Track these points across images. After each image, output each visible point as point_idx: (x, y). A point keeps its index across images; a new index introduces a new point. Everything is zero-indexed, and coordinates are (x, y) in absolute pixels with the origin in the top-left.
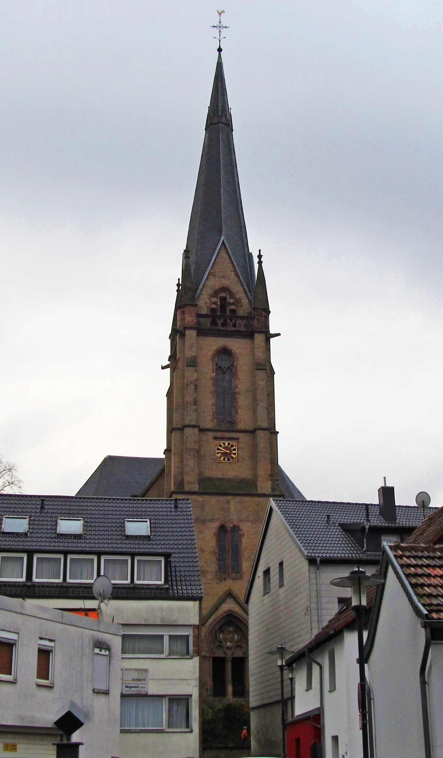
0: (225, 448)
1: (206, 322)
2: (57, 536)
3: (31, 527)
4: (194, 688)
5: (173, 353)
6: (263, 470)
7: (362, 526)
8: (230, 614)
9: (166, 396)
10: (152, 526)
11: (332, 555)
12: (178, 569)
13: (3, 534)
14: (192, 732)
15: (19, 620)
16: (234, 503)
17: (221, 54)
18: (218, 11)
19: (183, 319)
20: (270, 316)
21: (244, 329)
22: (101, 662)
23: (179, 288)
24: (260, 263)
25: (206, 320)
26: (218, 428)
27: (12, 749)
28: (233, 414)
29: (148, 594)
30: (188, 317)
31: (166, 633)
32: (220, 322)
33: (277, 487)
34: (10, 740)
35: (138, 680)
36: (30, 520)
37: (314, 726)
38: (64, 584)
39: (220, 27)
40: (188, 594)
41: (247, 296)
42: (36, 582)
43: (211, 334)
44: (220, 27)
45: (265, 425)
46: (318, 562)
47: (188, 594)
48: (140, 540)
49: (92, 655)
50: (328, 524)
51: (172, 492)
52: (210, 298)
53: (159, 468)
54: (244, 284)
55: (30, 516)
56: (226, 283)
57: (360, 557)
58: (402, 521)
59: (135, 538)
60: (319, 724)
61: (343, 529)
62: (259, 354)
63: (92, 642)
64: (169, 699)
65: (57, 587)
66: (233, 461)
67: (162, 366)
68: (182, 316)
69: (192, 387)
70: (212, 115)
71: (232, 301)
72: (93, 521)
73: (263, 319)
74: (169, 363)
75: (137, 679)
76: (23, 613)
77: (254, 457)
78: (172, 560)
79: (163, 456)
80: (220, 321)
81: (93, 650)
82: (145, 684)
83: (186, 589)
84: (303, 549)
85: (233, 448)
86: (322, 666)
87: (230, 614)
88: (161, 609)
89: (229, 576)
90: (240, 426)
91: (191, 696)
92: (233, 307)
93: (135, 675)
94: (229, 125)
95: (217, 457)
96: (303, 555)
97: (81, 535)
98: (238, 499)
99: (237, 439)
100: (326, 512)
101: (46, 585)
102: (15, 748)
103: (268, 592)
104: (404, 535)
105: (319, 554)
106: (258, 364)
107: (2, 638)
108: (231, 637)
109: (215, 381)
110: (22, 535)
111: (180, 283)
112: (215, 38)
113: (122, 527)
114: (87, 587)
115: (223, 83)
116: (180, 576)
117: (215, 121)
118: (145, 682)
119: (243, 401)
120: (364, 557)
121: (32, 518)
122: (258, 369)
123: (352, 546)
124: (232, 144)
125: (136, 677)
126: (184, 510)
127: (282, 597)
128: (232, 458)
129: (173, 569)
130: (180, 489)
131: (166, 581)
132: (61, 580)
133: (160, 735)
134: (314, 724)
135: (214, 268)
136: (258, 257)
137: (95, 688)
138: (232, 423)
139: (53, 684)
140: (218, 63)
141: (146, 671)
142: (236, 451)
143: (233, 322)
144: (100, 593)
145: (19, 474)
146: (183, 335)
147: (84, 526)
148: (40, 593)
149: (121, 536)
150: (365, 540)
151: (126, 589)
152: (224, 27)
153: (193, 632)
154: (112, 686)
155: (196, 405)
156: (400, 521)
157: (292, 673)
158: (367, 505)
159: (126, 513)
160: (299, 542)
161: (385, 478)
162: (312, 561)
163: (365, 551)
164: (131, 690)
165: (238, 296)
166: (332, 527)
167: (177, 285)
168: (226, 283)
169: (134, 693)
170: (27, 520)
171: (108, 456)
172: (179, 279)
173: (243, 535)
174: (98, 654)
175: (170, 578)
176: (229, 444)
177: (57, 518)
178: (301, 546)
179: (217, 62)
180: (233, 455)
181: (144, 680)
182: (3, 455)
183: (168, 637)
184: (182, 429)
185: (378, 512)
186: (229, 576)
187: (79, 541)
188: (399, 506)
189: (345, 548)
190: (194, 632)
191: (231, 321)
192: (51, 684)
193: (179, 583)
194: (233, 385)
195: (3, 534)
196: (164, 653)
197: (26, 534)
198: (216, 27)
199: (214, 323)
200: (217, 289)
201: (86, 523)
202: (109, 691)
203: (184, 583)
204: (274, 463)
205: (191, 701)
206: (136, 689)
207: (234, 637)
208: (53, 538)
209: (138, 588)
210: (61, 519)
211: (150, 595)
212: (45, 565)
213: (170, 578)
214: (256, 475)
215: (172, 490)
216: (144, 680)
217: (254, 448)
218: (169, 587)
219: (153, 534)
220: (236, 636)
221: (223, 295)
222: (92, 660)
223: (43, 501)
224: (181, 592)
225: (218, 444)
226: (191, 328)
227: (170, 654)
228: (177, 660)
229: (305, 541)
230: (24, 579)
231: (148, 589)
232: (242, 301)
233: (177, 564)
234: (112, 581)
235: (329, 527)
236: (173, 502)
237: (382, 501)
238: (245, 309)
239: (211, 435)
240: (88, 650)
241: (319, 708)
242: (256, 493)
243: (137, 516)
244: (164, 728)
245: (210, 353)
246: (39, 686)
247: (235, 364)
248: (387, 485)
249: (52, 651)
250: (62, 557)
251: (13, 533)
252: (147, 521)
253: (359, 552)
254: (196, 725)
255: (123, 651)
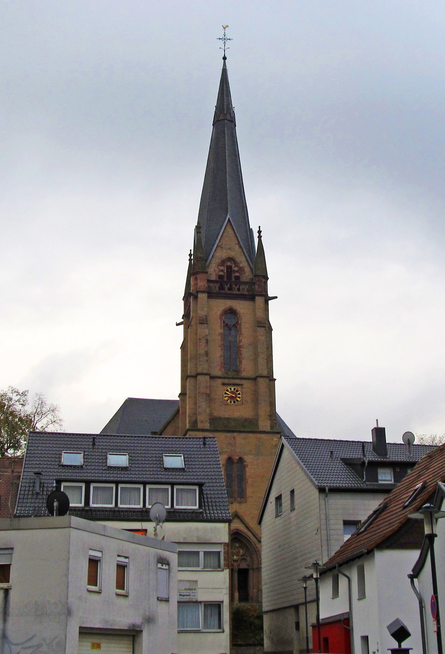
0: (232, 392)
1: (215, 287)
2: (108, 468)
3: (85, 460)
4: (225, 595)
5: (186, 312)
6: (263, 410)
7: (362, 460)
8: (236, 532)
9: (181, 348)
10: (186, 460)
11: (335, 485)
12: (209, 496)
13: (63, 467)
14: (223, 632)
15: (102, 541)
16: (240, 438)
17: (225, 62)
18: (223, 26)
19: (196, 284)
20: (268, 281)
21: (247, 293)
22: (163, 575)
23: (190, 257)
24: (260, 237)
25: (215, 285)
26: (225, 375)
27: (97, 647)
28: (238, 364)
29: (186, 517)
30: (200, 282)
31: (202, 550)
32: (226, 287)
33: (275, 425)
34: (96, 640)
35: (189, 589)
36: (84, 455)
37: (345, 628)
38: (116, 509)
39: (225, 39)
40: (219, 517)
41: (249, 265)
42: (93, 507)
43: (222, 297)
44: (225, 39)
45: (265, 373)
46: (327, 491)
47: (223, 517)
48: (180, 472)
49: (156, 569)
50: (332, 458)
51: (188, 429)
52: (218, 267)
53: (176, 408)
54: (247, 255)
55: (84, 452)
56: (232, 254)
57: (361, 486)
58: (392, 457)
59: (179, 470)
60: (349, 626)
61: (344, 463)
62: (260, 313)
63: (156, 559)
64: (204, 604)
65: (110, 511)
66: (238, 403)
67: (177, 323)
68: (195, 282)
69: (204, 341)
70: (218, 113)
71: (236, 269)
72: (136, 455)
73: (263, 284)
74: (183, 320)
75: (189, 589)
76: (105, 535)
77: (256, 401)
78: (204, 488)
79: (178, 399)
80: (227, 286)
81: (157, 565)
82: (195, 593)
83: (217, 513)
84: (314, 479)
85: (238, 393)
86: (350, 578)
87: (236, 532)
88: (197, 529)
89: (235, 500)
90: (244, 374)
91: (222, 602)
92: (237, 274)
93: (187, 586)
94: (233, 121)
95: (225, 400)
96: (314, 485)
97: (127, 467)
98: (243, 435)
99: (242, 385)
100: (329, 448)
101: (101, 509)
102: (100, 646)
103: (279, 515)
104: (397, 468)
105: (327, 484)
106: (259, 322)
107: (91, 556)
108: (237, 552)
109: (224, 336)
110: (79, 467)
111: (192, 253)
112: (220, 48)
113: (161, 461)
114: (135, 511)
115: (227, 86)
116: (212, 502)
117: (222, 118)
118: (195, 591)
119: (246, 353)
120: (364, 486)
121: (86, 453)
122: (258, 326)
123: (354, 477)
124: (236, 138)
125: (188, 587)
126: (211, 446)
127: (293, 519)
128: (237, 401)
129: (205, 496)
130: (194, 427)
131: (200, 506)
132: (113, 505)
133: (197, 635)
134: (345, 626)
135: (221, 241)
136: (258, 232)
137: (159, 596)
138: (238, 371)
139: (128, 594)
140: (223, 69)
141: (196, 582)
142: (240, 395)
143: (238, 286)
144: (157, 517)
145: (61, 414)
146: (196, 297)
147: (129, 460)
148: (97, 516)
149: (160, 468)
150: (364, 472)
151: (195, 514)
152: (228, 39)
153: (224, 549)
154: (171, 595)
155: (207, 357)
156: (390, 456)
157: (306, 583)
158: (363, 443)
159: (164, 449)
160: (310, 474)
161: (377, 420)
162: (322, 490)
163: (364, 481)
164: (184, 597)
165: (241, 265)
166: (336, 462)
167: (189, 255)
168: (232, 254)
169: (186, 600)
170: (82, 454)
171: (128, 398)
172: (191, 250)
173: (247, 466)
174: (160, 568)
175: (203, 504)
176: (234, 389)
177: (107, 453)
178: (312, 477)
179: (222, 69)
180: (238, 399)
181: (195, 589)
182: (47, 398)
183: (203, 553)
184: (195, 377)
185: (372, 448)
186: (235, 500)
187: (126, 473)
188: (388, 444)
189: (348, 479)
190: (224, 549)
191: (236, 285)
192: (126, 593)
193: (211, 508)
194: (238, 340)
195: (63, 467)
196: (200, 567)
197: (82, 467)
198: (221, 39)
199: (222, 288)
200: (224, 259)
201: (131, 457)
202: (169, 598)
203: (215, 508)
204: (272, 405)
205: (223, 607)
206: (188, 597)
207: (240, 552)
208: (104, 470)
209: (178, 512)
210: (110, 454)
211: (104, 516)
212: (100, 493)
213: (203, 504)
214: (257, 415)
215: (187, 427)
216: (195, 589)
217: (256, 393)
218: (203, 511)
219: (187, 466)
220: (241, 551)
221: (229, 264)
222: (157, 573)
223: (94, 438)
224: (213, 515)
225: (226, 389)
226: (203, 292)
227: (204, 568)
228: (209, 573)
229: (314, 473)
230: (82, 505)
231: (185, 513)
232: (245, 269)
233: (209, 492)
234: (165, 506)
235: (333, 461)
236: (202, 440)
237: (375, 439)
238: (247, 275)
239: (220, 381)
240: (153, 566)
241: (348, 612)
242: (258, 430)
243: (172, 452)
244: (201, 629)
245: (219, 313)
246: (117, 595)
247: (240, 322)
248: (379, 426)
249: (126, 566)
250: (114, 486)
251: (71, 466)
252: (181, 456)
253: (360, 482)
254: (227, 626)
255: (180, 565)
